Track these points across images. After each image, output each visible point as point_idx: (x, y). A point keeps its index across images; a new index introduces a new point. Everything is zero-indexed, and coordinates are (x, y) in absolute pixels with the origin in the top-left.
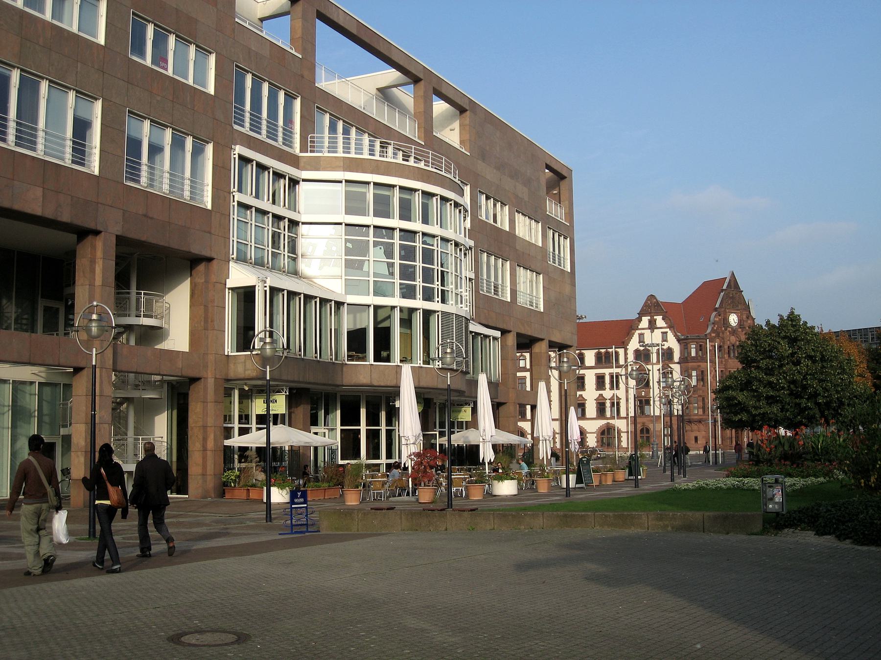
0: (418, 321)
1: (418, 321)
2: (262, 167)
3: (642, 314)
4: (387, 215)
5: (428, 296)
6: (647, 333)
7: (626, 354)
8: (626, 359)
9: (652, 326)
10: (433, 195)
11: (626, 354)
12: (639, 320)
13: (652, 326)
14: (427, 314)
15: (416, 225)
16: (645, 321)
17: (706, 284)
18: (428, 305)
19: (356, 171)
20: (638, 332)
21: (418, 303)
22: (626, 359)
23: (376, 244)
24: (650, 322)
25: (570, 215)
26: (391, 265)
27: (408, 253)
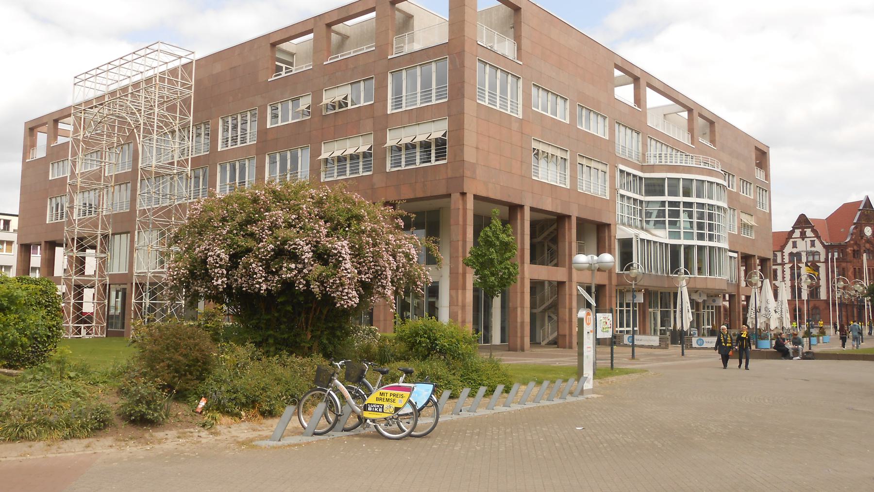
0: (707, 252)
1: (707, 252)
2: (712, 183)
3: (794, 228)
4: (677, 195)
5: (701, 237)
6: (799, 241)
7: (783, 256)
8: (783, 259)
9: (803, 236)
10: (703, 181)
11: (783, 256)
12: (792, 232)
13: (803, 236)
14: (701, 248)
15: (693, 199)
16: (797, 233)
17: (845, 205)
18: (701, 243)
19: (699, 174)
20: (791, 240)
21: (696, 242)
22: (783, 259)
23: (684, 211)
24: (801, 233)
25: (767, 176)
26: (691, 223)
27: (701, 216)
